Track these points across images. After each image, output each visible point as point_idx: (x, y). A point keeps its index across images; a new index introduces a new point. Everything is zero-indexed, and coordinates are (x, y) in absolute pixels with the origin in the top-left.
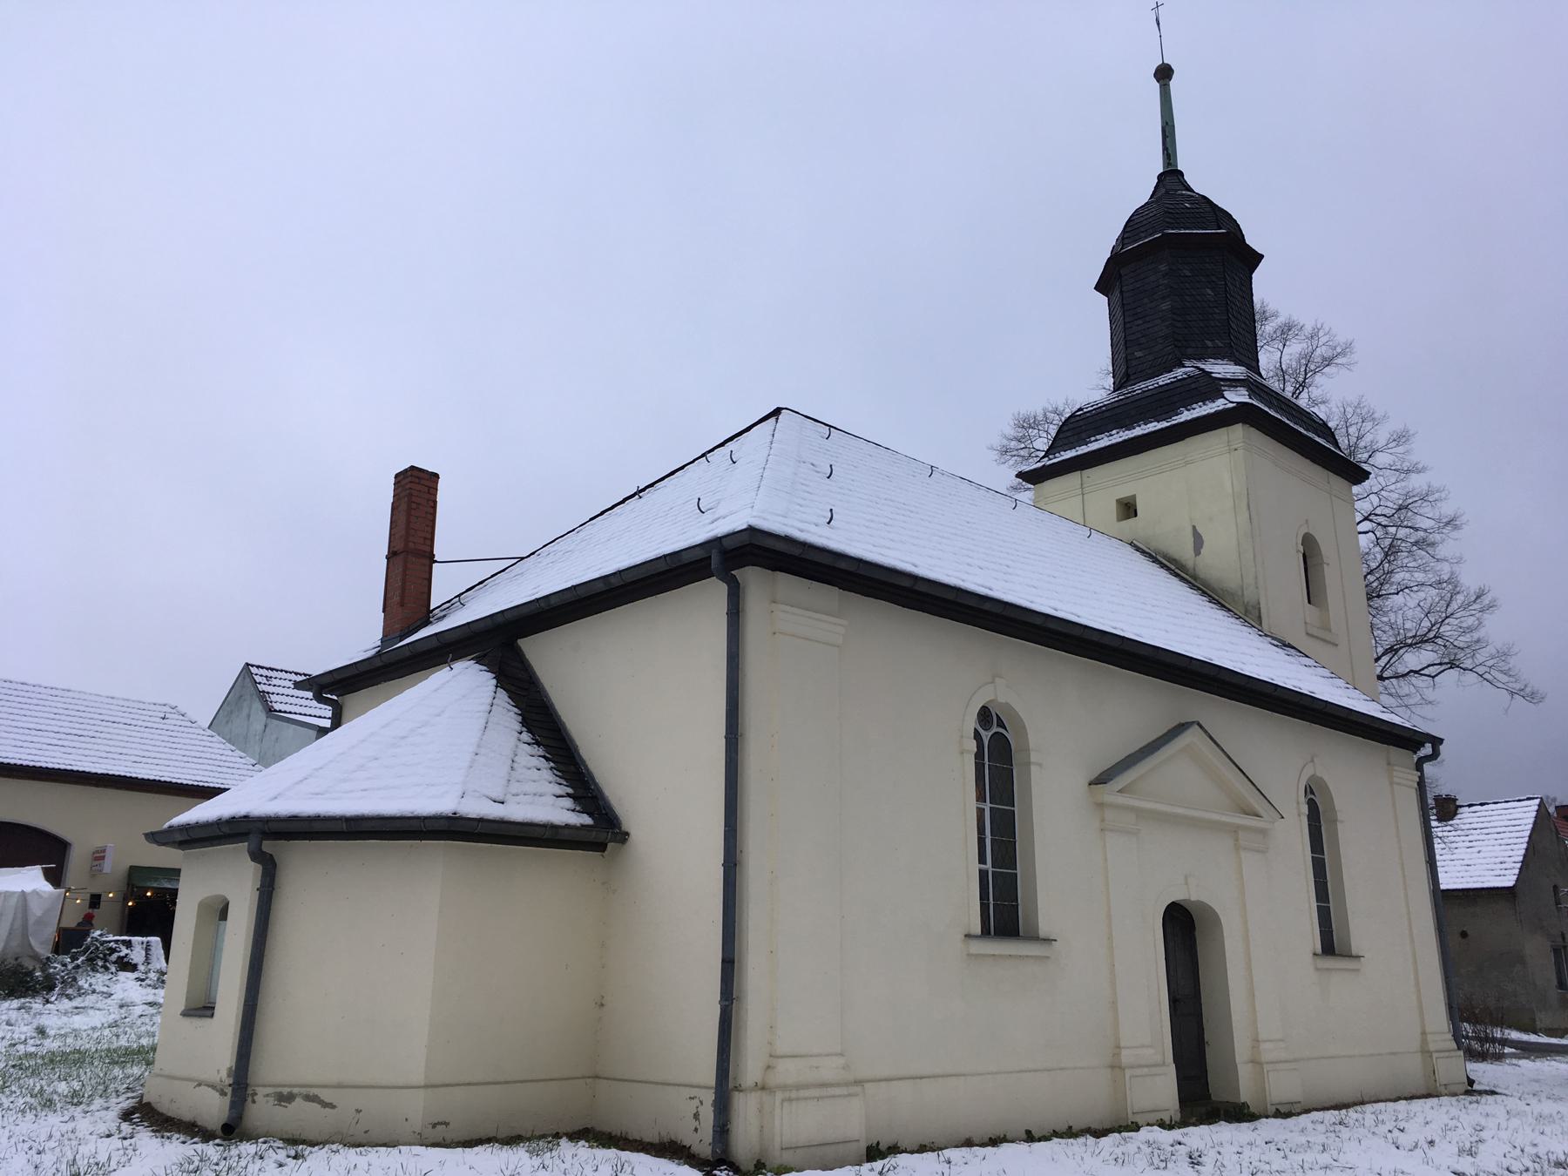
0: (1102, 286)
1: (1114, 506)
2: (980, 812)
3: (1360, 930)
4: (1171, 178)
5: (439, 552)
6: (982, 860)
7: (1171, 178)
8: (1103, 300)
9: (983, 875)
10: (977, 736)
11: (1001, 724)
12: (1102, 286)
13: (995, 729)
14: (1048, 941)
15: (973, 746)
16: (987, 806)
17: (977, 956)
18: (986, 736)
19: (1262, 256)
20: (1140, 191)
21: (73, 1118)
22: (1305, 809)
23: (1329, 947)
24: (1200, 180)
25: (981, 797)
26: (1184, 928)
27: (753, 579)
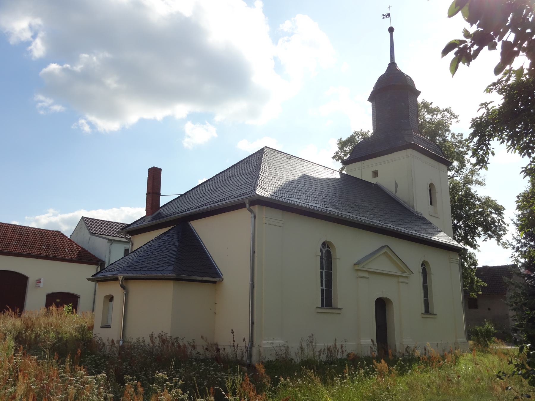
0: (370, 99)
1: (371, 173)
2: (322, 273)
3: (437, 306)
4: (392, 65)
5: (162, 192)
6: (322, 286)
7: (392, 65)
8: (370, 104)
9: (322, 290)
10: (321, 251)
11: (328, 247)
12: (370, 99)
13: (327, 249)
14: (340, 309)
15: (320, 254)
16: (324, 271)
17: (360, 277)
18: (324, 251)
19: (420, 92)
20: (383, 69)
21: (359, 398)
22: (421, 270)
23: (427, 311)
24: (403, 67)
25: (322, 268)
26: (382, 305)
27: (256, 208)
